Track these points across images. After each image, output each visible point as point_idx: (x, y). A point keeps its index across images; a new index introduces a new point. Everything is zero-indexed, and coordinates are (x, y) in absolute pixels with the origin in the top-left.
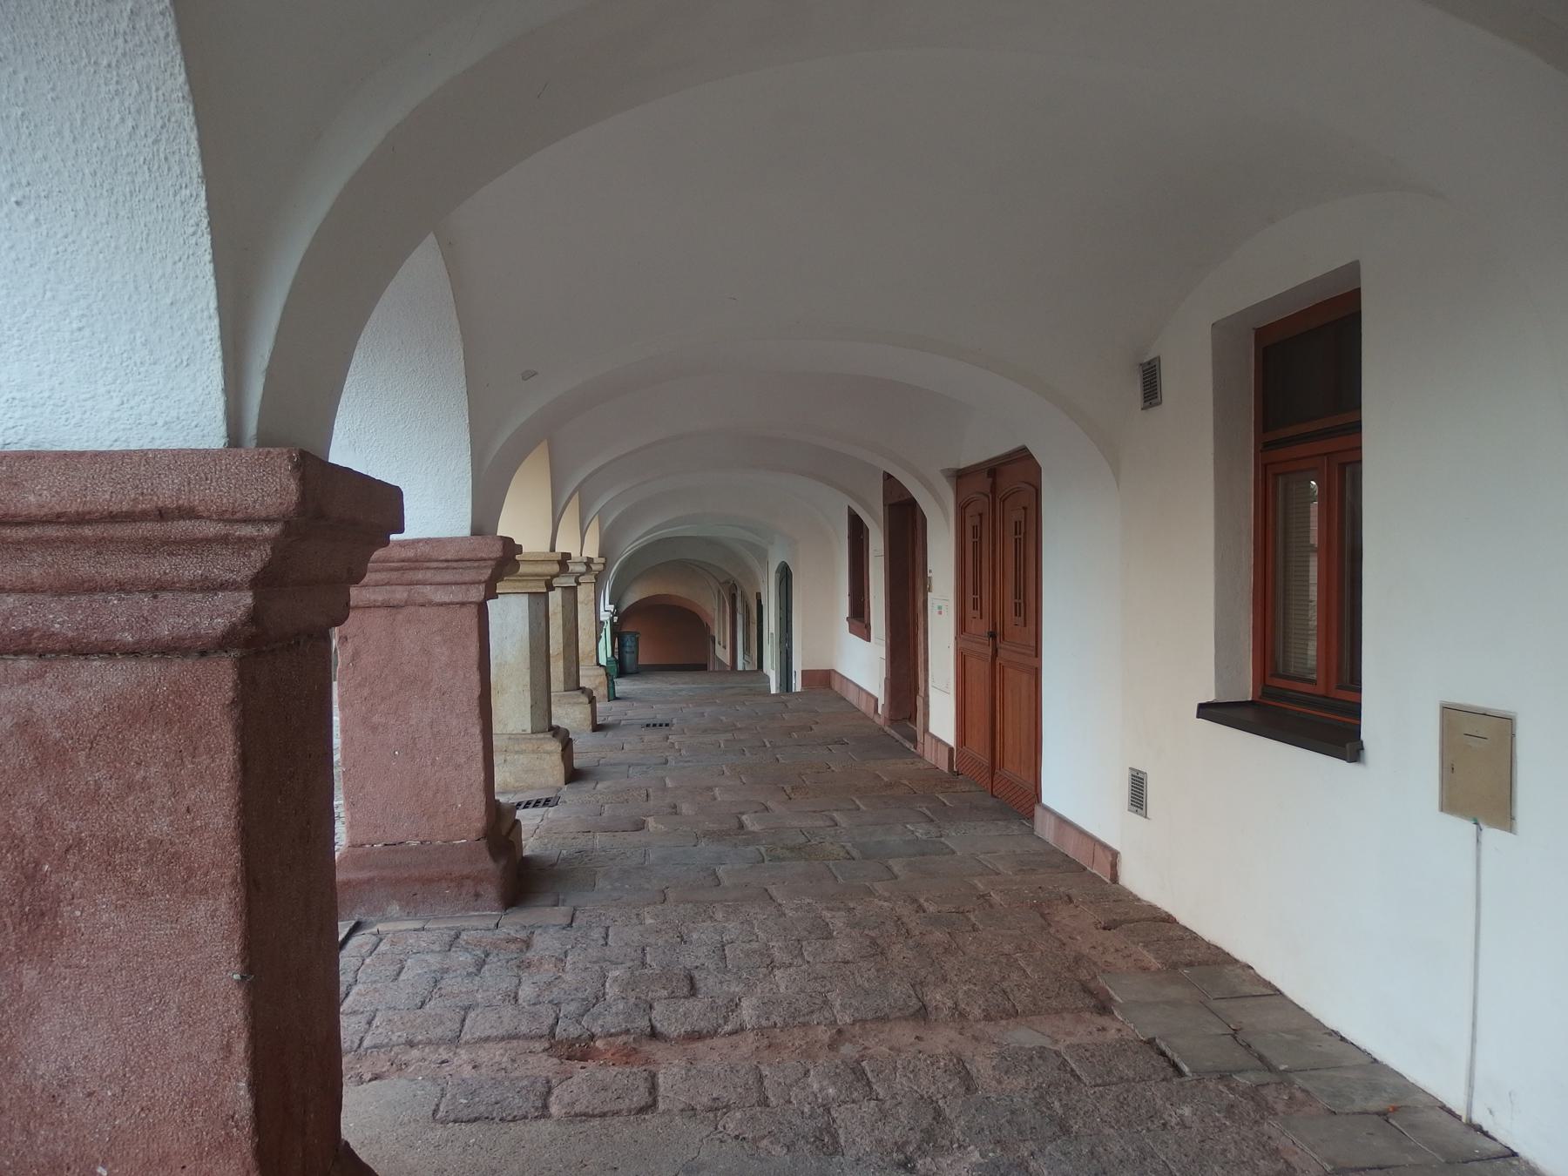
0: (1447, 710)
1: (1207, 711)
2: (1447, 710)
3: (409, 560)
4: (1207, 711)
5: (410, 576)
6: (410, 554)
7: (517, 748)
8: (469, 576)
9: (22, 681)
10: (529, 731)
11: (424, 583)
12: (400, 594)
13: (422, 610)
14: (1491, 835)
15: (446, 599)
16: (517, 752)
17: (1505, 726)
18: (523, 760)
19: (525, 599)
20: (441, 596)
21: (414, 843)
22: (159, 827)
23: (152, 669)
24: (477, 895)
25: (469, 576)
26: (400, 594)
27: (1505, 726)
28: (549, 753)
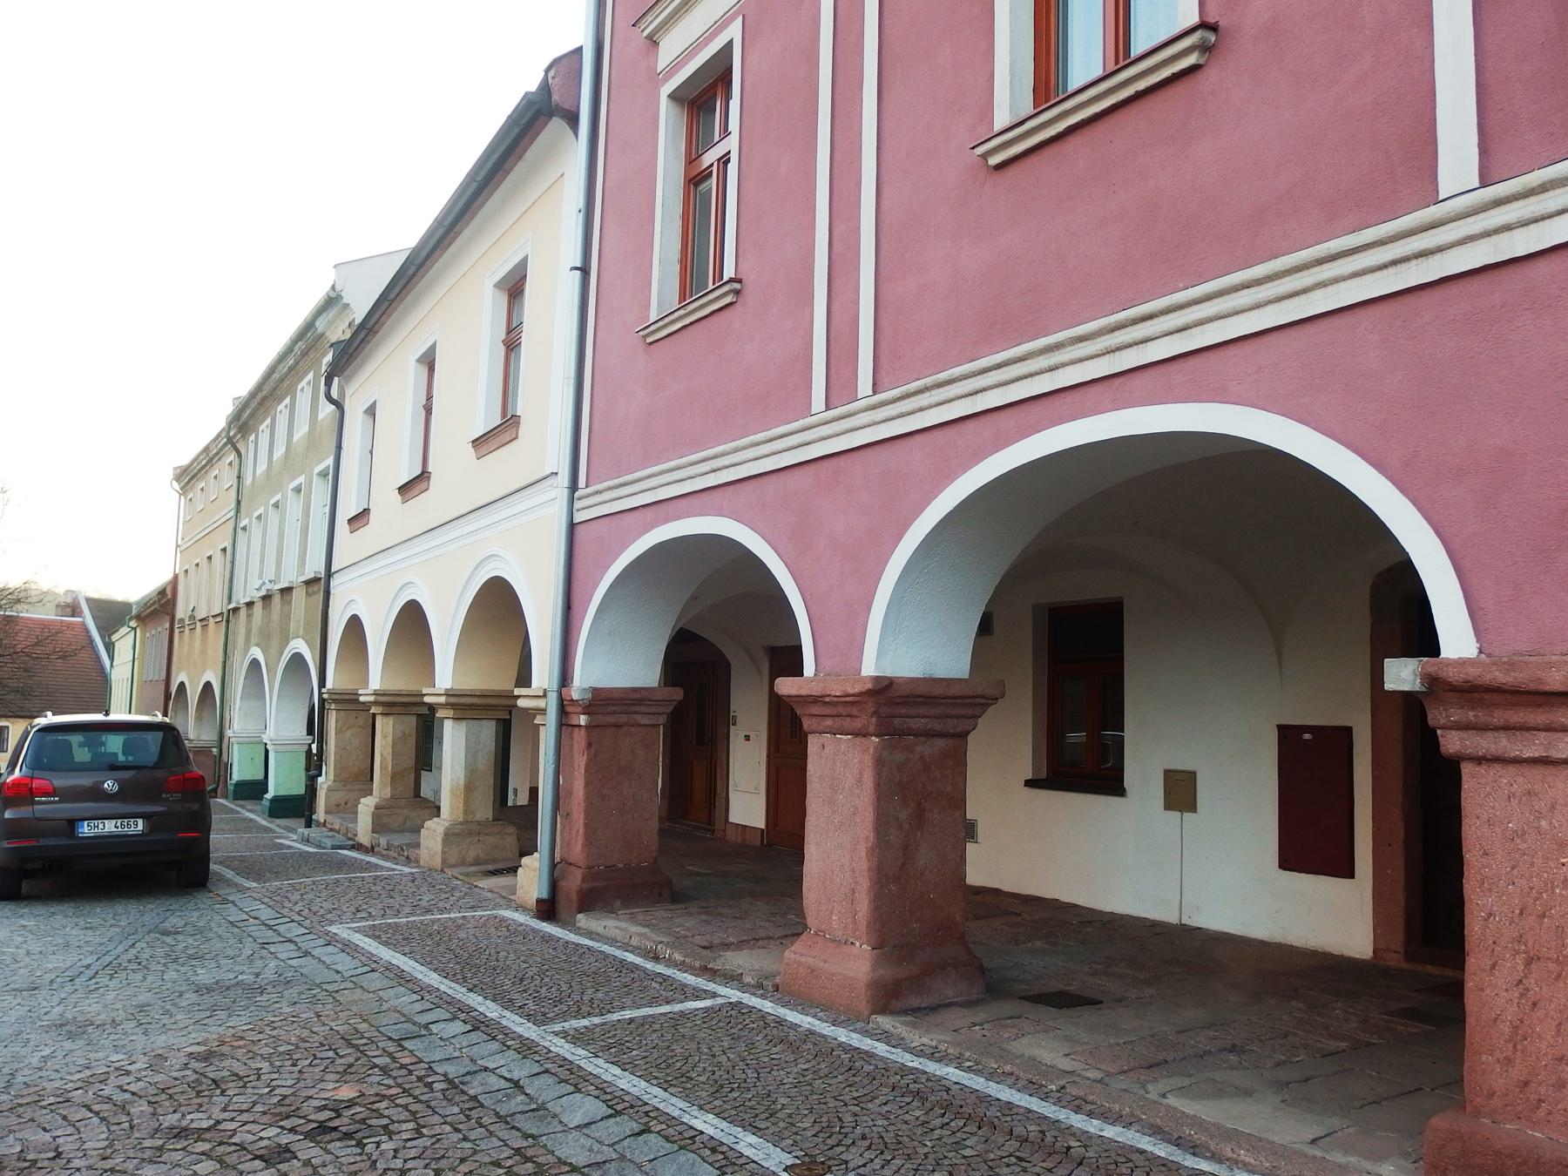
0: (1166, 772)
1: (1029, 783)
2: (1166, 772)
3: (637, 700)
4: (1029, 783)
5: (632, 709)
6: (638, 696)
7: (487, 832)
8: (661, 710)
9: (922, 744)
10: (491, 819)
11: (636, 713)
12: (624, 719)
13: (632, 729)
14: (1186, 815)
15: (646, 722)
16: (486, 834)
17: (1191, 776)
18: (491, 839)
19: (493, 723)
20: (644, 721)
21: (621, 866)
22: (949, 789)
23: (950, 741)
24: (660, 894)
25: (661, 710)
26: (624, 719)
27: (1191, 776)
28: (510, 834)
